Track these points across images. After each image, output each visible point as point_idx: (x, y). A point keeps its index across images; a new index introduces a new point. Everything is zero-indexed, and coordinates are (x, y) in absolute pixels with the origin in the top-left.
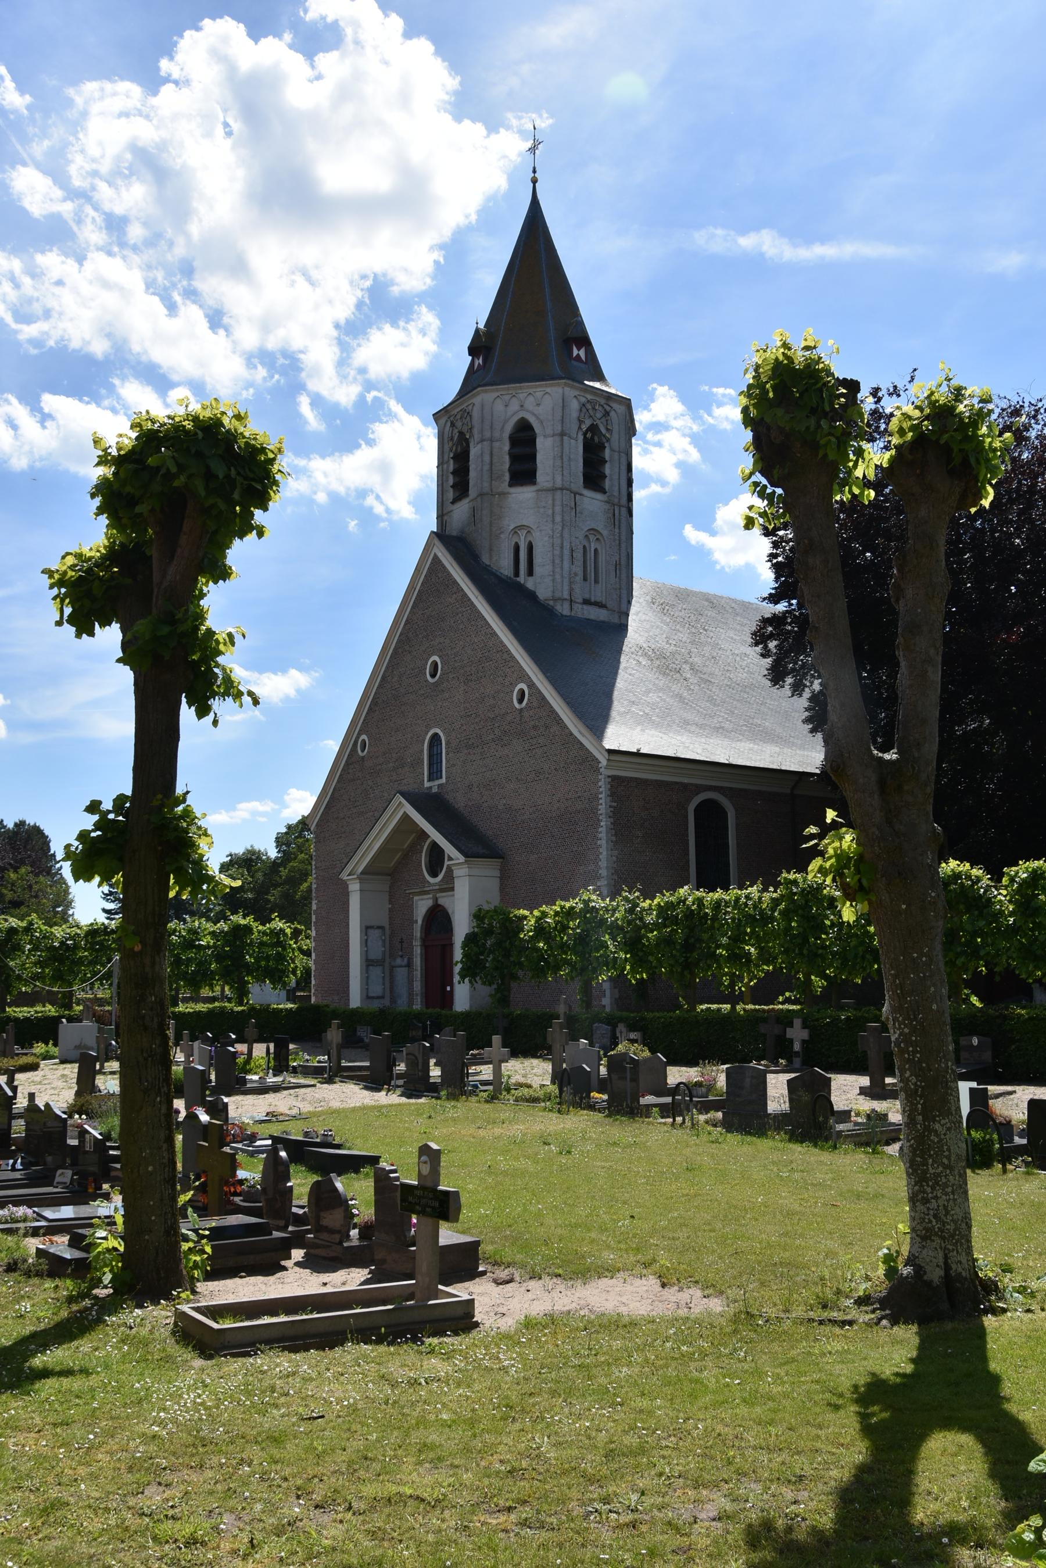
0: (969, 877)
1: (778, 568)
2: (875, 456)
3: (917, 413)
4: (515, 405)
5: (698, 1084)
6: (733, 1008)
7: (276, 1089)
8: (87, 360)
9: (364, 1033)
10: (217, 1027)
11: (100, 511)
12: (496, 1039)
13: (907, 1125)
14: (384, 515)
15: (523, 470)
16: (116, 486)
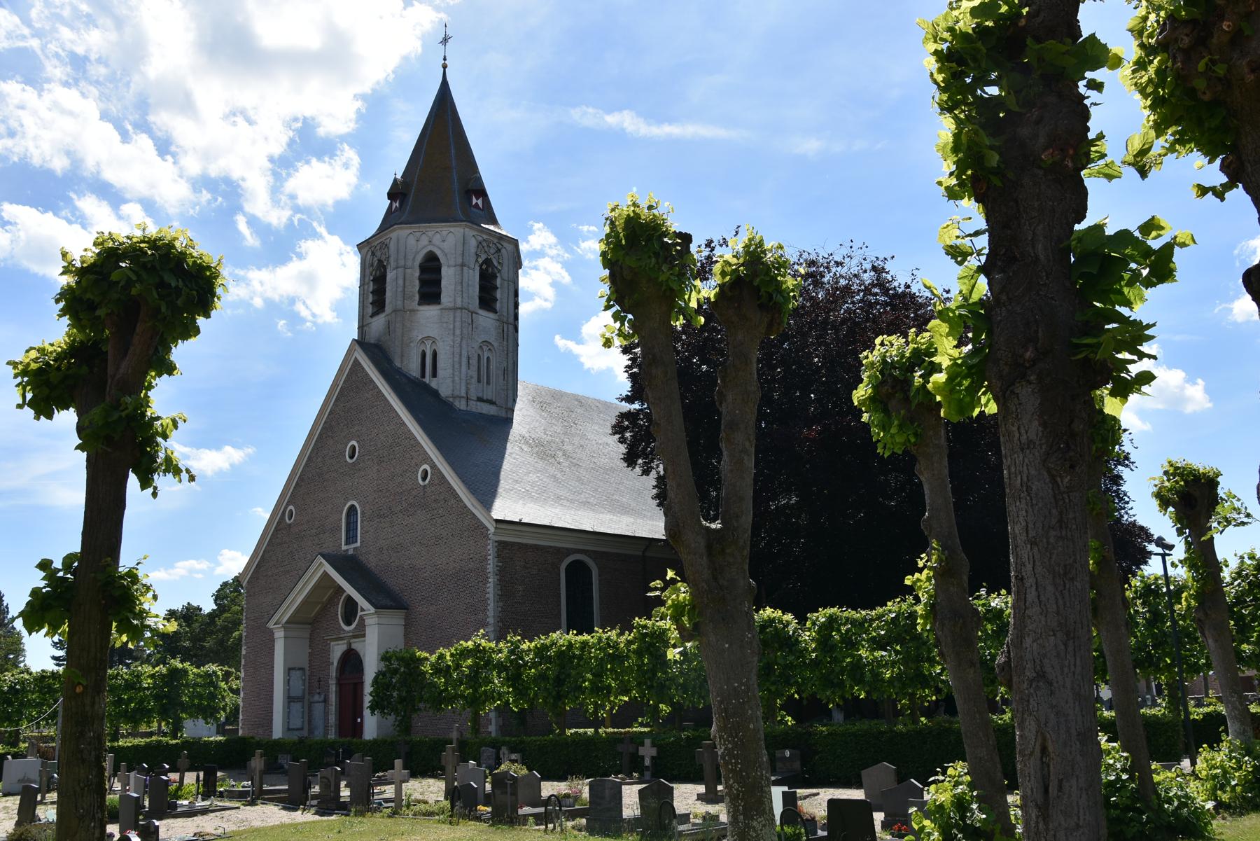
0: (781, 622)
1: (633, 377)
2: (705, 290)
3: (734, 261)
4: (424, 241)
5: (567, 796)
6: (596, 731)
7: (204, 812)
8: (47, 174)
9: (285, 760)
10: (152, 759)
11: (63, 312)
12: (398, 763)
13: (731, 823)
14: (310, 318)
15: (430, 292)
16: (77, 293)
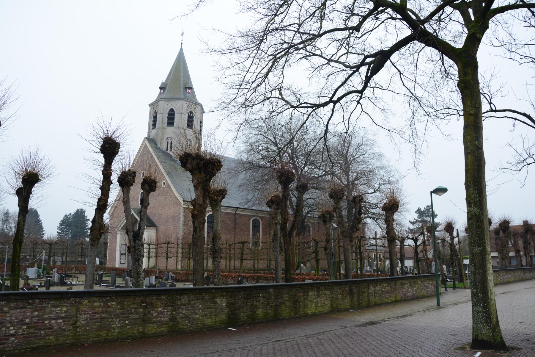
15: (171, 122)
